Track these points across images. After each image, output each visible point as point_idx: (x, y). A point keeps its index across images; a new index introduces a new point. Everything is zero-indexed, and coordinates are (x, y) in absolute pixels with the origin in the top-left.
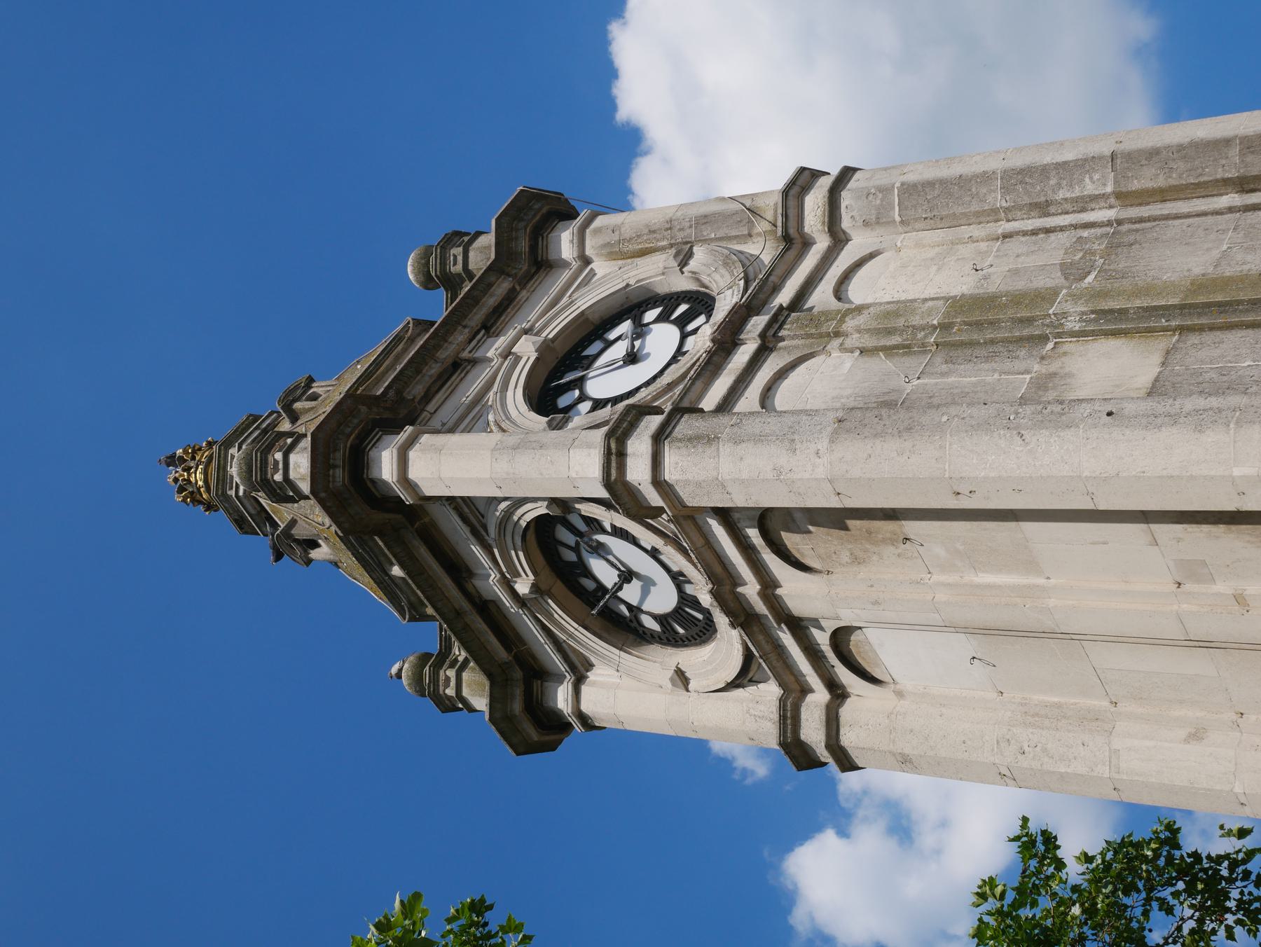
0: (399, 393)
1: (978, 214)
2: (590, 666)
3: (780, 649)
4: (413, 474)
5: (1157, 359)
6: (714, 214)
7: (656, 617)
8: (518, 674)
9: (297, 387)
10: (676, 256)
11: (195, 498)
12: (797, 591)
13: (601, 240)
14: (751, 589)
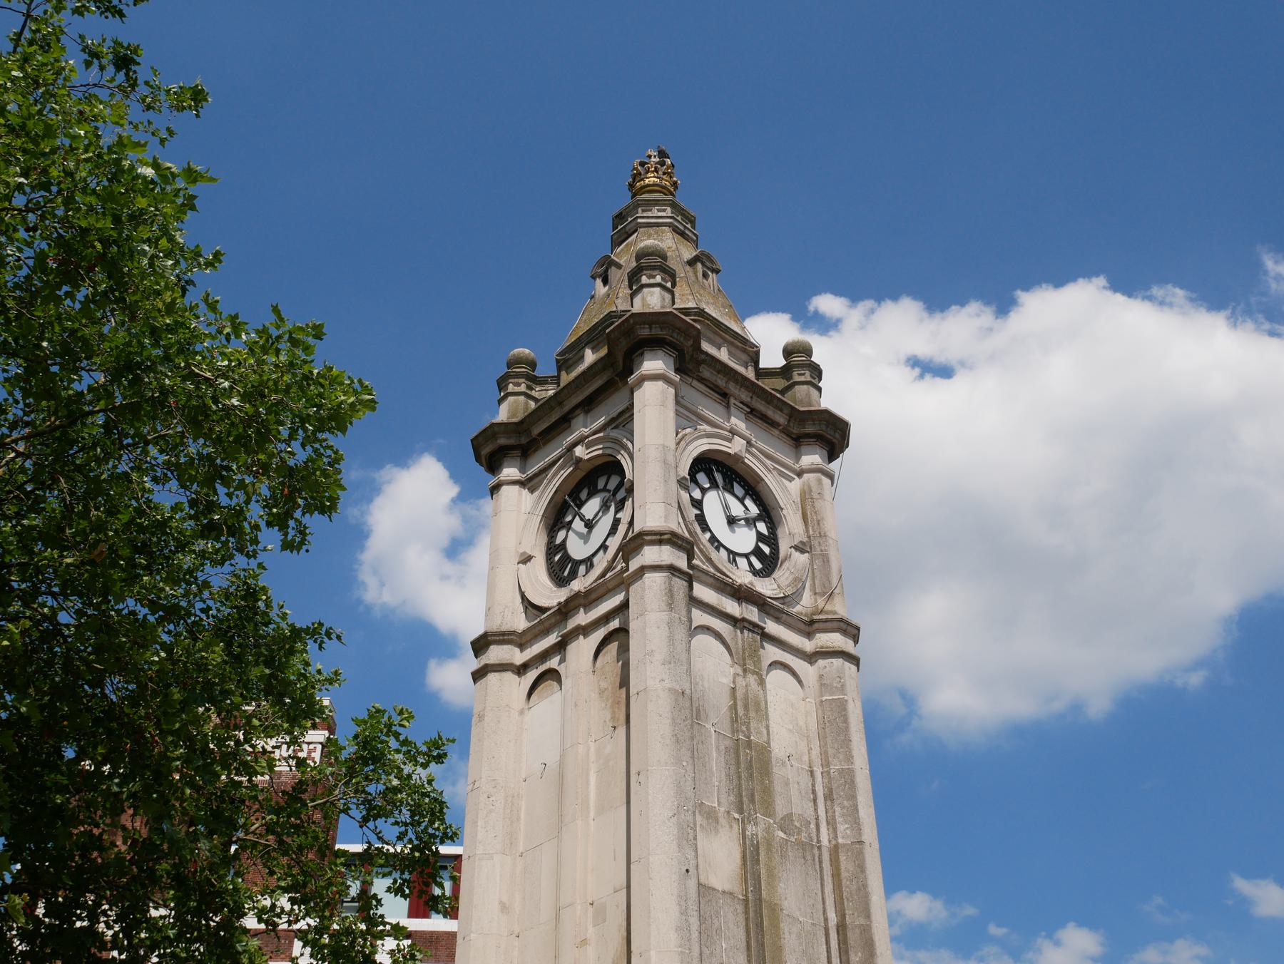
0: (704, 361)
1: (826, 753)
2: (532, 491)
3: (546, 632)
4: (647, 384)
5: (727, 887)
6: (829, 567)
7: (564, 541)
8: (524, 441)
9: (712, 261)
10: (801, 542)
11: (637, 176)
12: (583, 648)
13: (814, 485)
14: (582, 618)
